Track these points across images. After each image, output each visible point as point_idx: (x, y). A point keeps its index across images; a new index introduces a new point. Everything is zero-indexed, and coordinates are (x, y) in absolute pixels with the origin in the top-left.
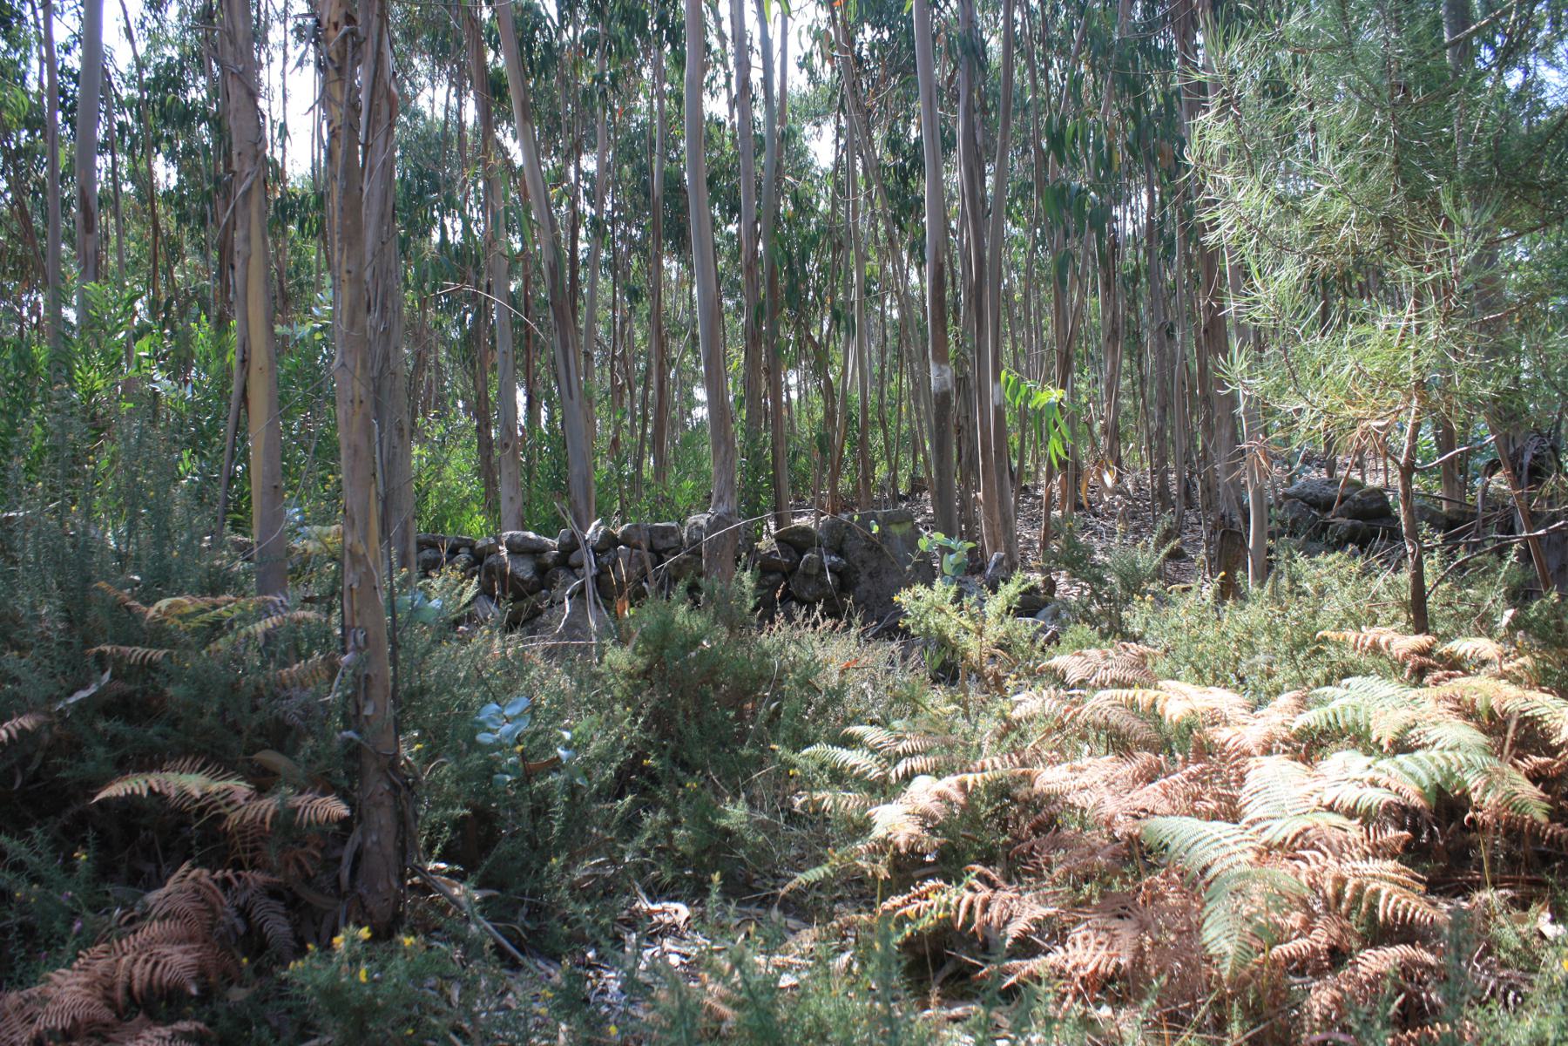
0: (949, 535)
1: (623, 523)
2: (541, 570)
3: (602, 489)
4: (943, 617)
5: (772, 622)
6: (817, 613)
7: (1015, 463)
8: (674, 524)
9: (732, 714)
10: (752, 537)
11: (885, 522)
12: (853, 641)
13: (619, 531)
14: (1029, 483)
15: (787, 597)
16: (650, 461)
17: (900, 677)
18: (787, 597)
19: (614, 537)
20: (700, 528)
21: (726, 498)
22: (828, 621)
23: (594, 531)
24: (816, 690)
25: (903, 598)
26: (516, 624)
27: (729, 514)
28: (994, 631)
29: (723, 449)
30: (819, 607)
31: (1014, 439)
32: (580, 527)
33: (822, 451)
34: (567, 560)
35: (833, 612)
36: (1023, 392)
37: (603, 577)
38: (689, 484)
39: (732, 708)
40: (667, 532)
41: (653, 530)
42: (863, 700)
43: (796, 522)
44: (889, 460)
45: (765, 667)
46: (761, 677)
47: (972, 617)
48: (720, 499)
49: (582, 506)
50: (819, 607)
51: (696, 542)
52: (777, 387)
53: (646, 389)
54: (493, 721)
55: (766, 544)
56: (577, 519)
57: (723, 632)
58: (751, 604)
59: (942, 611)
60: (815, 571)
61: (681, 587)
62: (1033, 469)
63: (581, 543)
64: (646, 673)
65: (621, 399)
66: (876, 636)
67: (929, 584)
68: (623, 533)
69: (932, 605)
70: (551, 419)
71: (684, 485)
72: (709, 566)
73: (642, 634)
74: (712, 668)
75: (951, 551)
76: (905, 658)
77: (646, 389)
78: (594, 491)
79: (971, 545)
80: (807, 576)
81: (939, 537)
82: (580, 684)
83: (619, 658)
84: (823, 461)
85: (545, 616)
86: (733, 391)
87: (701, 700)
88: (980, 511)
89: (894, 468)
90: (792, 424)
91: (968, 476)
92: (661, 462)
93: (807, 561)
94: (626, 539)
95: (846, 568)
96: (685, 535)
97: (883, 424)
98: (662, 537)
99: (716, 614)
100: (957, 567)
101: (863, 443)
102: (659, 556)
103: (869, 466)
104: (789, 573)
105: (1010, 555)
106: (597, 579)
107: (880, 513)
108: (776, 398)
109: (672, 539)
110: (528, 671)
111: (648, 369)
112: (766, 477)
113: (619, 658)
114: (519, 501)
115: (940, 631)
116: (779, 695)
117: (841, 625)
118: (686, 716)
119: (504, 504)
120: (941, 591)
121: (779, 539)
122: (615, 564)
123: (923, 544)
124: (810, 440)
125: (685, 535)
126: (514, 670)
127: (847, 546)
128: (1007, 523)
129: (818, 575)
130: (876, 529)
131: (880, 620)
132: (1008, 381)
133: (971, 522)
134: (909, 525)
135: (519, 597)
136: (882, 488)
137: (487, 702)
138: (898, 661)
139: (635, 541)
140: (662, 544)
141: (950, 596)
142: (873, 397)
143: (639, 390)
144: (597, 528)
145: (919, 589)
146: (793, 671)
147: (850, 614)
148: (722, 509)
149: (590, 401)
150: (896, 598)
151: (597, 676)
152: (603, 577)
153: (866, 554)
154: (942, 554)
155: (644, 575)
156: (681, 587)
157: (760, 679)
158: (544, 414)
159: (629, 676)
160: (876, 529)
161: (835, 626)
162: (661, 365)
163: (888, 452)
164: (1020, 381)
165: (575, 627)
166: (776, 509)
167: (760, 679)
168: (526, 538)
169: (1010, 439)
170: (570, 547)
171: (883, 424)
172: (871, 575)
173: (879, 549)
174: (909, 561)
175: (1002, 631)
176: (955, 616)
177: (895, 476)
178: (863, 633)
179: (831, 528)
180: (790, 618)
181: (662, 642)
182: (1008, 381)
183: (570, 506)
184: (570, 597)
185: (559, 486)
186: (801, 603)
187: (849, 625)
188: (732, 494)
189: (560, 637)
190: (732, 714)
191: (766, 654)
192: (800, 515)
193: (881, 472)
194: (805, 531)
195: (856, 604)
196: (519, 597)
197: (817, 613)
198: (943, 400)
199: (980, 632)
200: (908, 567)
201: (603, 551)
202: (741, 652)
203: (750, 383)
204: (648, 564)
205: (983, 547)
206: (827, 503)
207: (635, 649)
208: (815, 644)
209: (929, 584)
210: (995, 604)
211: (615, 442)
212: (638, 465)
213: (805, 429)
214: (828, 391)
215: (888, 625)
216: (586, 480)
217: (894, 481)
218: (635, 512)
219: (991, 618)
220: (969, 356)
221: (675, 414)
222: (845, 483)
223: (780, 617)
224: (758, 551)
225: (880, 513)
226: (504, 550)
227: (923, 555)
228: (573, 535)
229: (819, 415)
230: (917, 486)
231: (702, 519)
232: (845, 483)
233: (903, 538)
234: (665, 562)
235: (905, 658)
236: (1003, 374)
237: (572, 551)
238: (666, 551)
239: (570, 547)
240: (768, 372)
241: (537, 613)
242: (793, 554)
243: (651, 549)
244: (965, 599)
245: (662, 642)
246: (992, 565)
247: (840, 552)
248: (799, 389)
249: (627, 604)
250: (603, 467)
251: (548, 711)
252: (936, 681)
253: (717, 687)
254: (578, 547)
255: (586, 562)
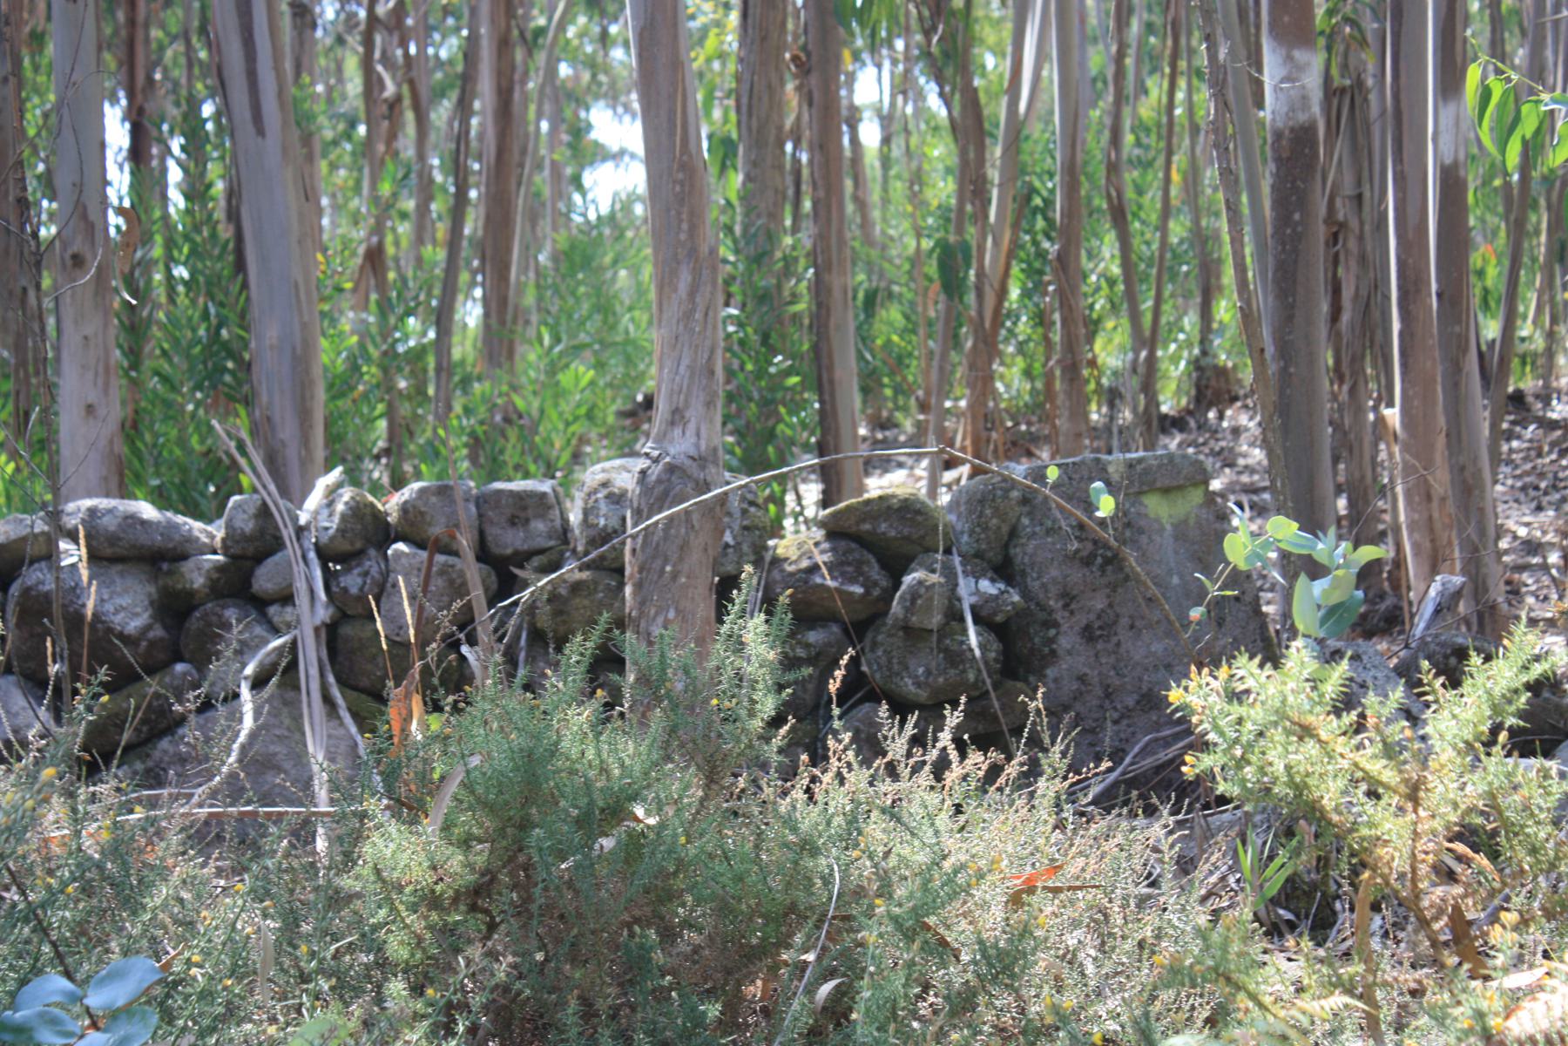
0: (1312, 523)
1: (398, 483)
2: (175, 608)
3: (341, 387)
4: (1311, 748)
5: (819, 757)
6: (945, 738)
7: (1491, 329)
8: (546, 486)
9: (713, 1010)
10: (760, 531)
11: (1136, 484)
12: (1044, 813)
13: (392, 505)
14: (1529, 384)
15: (858, 690)
16: (471, 314)
17: (1182, 918)
18: (858, 690)
19: (379, 518)
20: (617, 499)
21: (694, 413)
22: (975, 757)
23: (322, 502)
24: (943, 949)
25: (1196, 693)
26: (108, 758)
27: (701, 460)
28: (1453, 790)
29: (685, 279)
30: (953, 718)
31: (1487, 260)
32: (284, 491)
33: (952, 284)
34: (245, 579)
35: (986, 733)
36: (1528, 127)
37: (347, 630)
38: (580, 374)
39: (710, 994)
40: (524, 508)
41: (484, 502)
42: (1070, 977)
43: (876, 486)
44: (1135, 317)
45: (799, 879)
46: (793, 908)
47: (1390, 751)
48: (677, 417)
49: (287, 431)
50: (953, 718)
51: (603, 537)
52: (831, 114)
53: (464, 108)
54: (53, 1022)
55: (799, 540)
56: (274, 463)
57: (684, 783)
58: (768, 706)
59: (1305, 732)
60: (936, 620)
61: (578, 651)
62: (1539, 343)
63: (287, 533)
64: (476, 896)
65: (392, 136)
66: (1106, 802)
67: (1272, 656)
68: (405, 508)
69: (1281, 714)
70: (196, 191)
71: (565, 379)
72: (642, 603)
73: (467, 785)
74: (654, 882)
75: (1316, 570)
76: (1185, 866)
77: (464, 108)
78: (321, 394)
79: (1368, 553)
80: (912, 634)
81: (1284, 530)
82: (291, 922)
83: (403, 851)
84: (952, 322)
85: (190, 734)
86: (715, 119)
87: (634, 970)
88: (1390, 455)
89: (1147, 339)
90: (866, 224)
91: (1357, 360)
92: (499, 307)
93: (914, 595)
94: (412, 528)
95: (1020, 613)
96: (575, 518)
97: (1119, 216)
98: (513, 522)
99: (672, 731)
100: (1332, 613)
101: (1067, 268)
102: (504, 575)
103: (1081, 329)
104: (862, 624)
105: (1477, 585)
106: (331, 634)
107: (1116, 461)
108: (825, 146)
109: (539, 526)
110: (145, 886)
111: (470, 52)
112: (789, 364)
113: (403, 851)
114: (114, 412)
115: (1299, 788)
116: (846, 966)
117: (1012, 770)
118: (588, 1012)
119: (70, 424)
120: (1296, 680)
121: (836, 531)
122: (383, 588)
123: (1238, 547)
124: (916, 260)
125: (575, 518)
126: (115, 884)
127: (1022, 554)
128: (1469, 490)
129: (943, 632)
130: (1106, 506)
131: (1117, 756)
132: (1486, 95)
133: (1363, 492)
134: (1196, 496)
135: (123, 680)
136: (1113, 397)
137: (36, 971)
138: (1168, 871)
139: (437, 530)
140: (509, 540)
141: (1332, 686)
142: (1095, 144)
143: (442, 113)
144: (332, 493)
145: (1247, 670)
146: (885, 891)
147: (1035, 742)
148: (681, 446)
149: (307, 139)
150: (1175, 695)
151: (338, 900)
152: (347, 630)
153: (1076, 575)
154: (1292, 577)
155: (466, 621)
156: (578, 651)
157: (787, 917)
158: (175, 174)
159: (432, 901)
160: (1106, 506)
161: (994, 771)
162: (503, 45)
163: (1131, 297)
164: (1518, 96)
165: (270, 766)
166: (821, 449)
167: (787, 917)
168: (133, 520)
169: (1475, 260)
170: (258, 545)
171: (1119, 216)
172: (1088, 634)
173: (1114, 560)
174: (1199, 596)
175: (1475, 789)
176: (1341, 745)
177: (1152, 361)
178: (1072, 796)
179: (978, 503)
180: (869, 746)
181: (519, 808)
182: (1486, 95)
183: (254, 431)
184: (258, 683)
185: (224, 370)
186: (901, 709)
187: (1032, 772)
188: (709, 404)
189: (233, 789)
190: (713, 1010)
191: (808, 847)
192: (886, 465)
193: (1110, 351)
194: (906, 510)
195: (1055, 711)
196: (123, 680)
197: (945, 738)
198: (1296, 151)
199: (1413, 793)
200: (1196, 613)
201: (349, 558)
202: (733, 837)
203: (754, 98)
204: (477, 594)
205: (1399, 563)
206: (961, 434)
207: (446, 828)
208: (943, 821)
209: (1272, 656)
210: (1457, 716)
211: (375, 258)
212: (443, 319)
213: (900, 232)
214: (969, 127)
215: (1151, 774)
216: (302, 359)
217: (1149, 377)
218: (432, 453)
219: (1445, 754)
220: (1370, 26)
221: (542, 181)
222: (1012, 381)
223: (840, 743)
224: (777, 561)
225: (1116, 461)
226: (72, 554)
227: (1237, 578)
228: (264, 512)
229: (942, 190)
230: (1211, 388)
231: (624, 474)
232: (1012, 381)
233: (1181, 531)
234: (530, 590)
235: (1185, 866)
236: (1473, 74)
237: (260, 558)
238: (522, 558)
239: (258, 545)
240: (803, 67)
241: (162, 723)
242: (875, 572)
243: (484, 554)
244: (1371, 699)
245: (519, 808)
246: (1428, 609)
247: (1004, 570)
248: (886, 120)
249: (417, 704)
250: (344, 333)
251: (206, 995)
252: (1275, 931)
253: (669, 935)
254: (277, 544)
255: (300, 586)
